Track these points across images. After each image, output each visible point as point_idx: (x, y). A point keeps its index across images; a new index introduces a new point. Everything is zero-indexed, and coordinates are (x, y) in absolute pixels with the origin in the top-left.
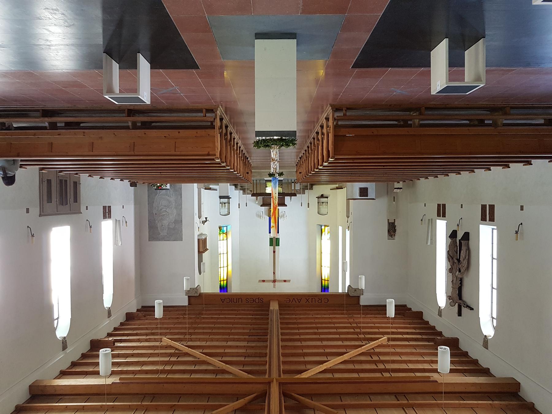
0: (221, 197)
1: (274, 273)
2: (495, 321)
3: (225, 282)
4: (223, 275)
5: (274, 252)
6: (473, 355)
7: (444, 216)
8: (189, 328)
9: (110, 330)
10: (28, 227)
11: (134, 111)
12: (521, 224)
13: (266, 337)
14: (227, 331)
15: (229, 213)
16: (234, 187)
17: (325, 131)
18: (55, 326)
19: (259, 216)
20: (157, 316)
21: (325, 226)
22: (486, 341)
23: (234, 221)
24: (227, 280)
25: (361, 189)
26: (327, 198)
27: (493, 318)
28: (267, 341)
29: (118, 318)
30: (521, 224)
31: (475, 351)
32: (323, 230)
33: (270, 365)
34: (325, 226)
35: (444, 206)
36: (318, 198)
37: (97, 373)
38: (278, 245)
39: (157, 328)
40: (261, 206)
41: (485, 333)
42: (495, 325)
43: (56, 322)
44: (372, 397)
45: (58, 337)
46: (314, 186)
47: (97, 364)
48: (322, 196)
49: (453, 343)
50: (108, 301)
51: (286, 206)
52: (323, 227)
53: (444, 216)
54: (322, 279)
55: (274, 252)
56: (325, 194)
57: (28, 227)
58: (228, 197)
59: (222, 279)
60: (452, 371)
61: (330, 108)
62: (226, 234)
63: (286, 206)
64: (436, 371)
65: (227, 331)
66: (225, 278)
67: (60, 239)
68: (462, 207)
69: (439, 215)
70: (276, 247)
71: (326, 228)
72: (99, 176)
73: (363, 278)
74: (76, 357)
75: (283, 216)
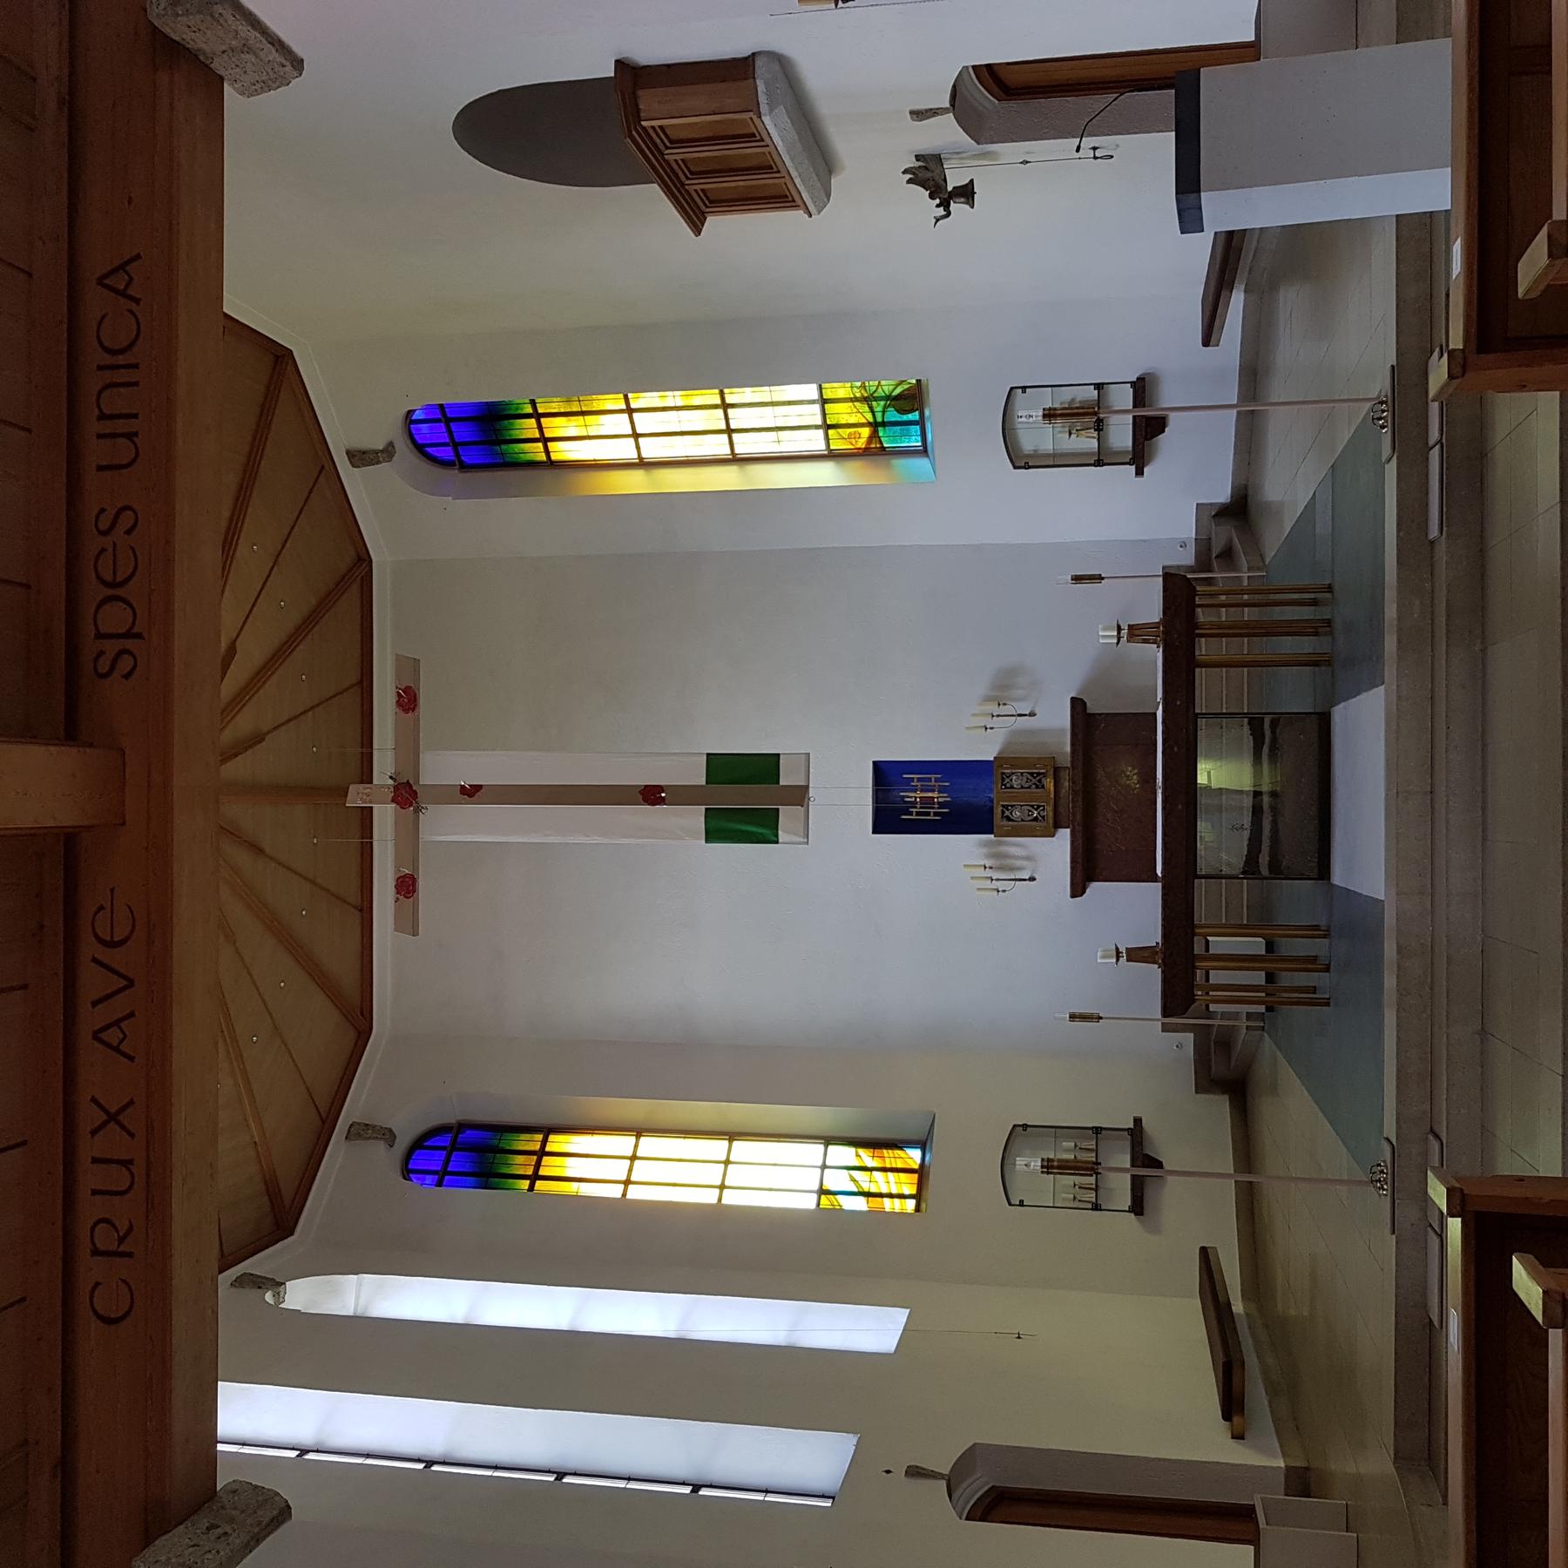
0: (1142, 388)
1: (471, 792)
3: (536, 452)
4: (590, 435)
5: (652, 795)
11: (1192, 607)
15: (1021, 460)
16: (1223, 495)
19: (1002, 690)
21: (922, 1173)
23: (969, 499)
24: (551, 464)
26: (1137, 1207)
32: (893, 1158)
34: (922, 1173)
36: (1136, 1133)
38: (721, 828)
40: (1077, 704)
46: (1220, 1106)
48: (1145, 1160)
51: (1078, 890)
52: (914, 1156)
54: (548, 1131)
55: (652, 795)
56: (1172, 1196)
58: (1139, 459)
59: (555, 427)
62: (873, 452)
63: (1078, 890)
66: (561, 452)
70: (696, 817)
71: (908, 1185)
75: (1003, 864)
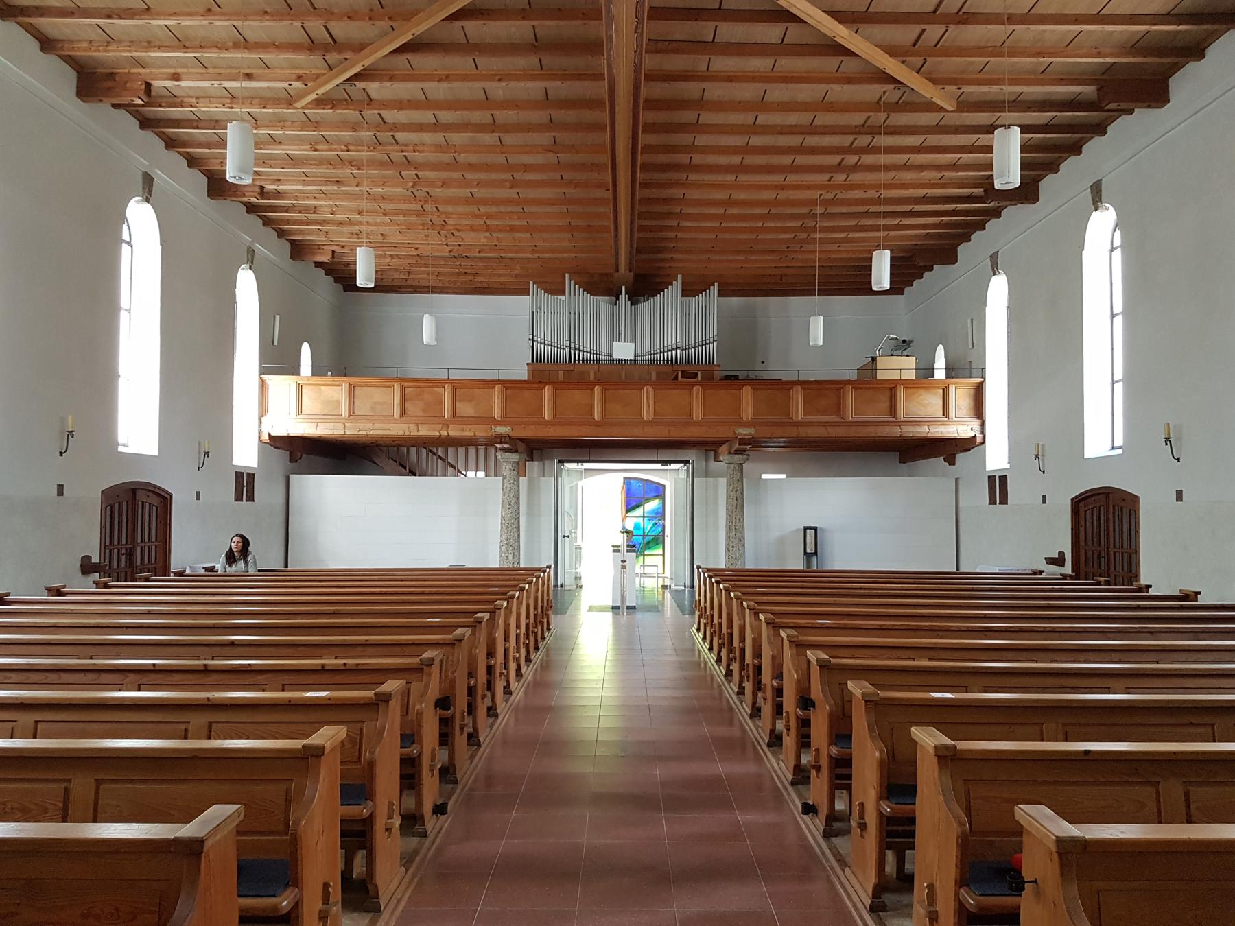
2: (125, 236)
6: (175, 160)
7: (239, 475)
8: (814, 229)
9: (992, 225)
10: (1178, 459)
12: (61, 454)
13: (641, 235)
14: (735, 211)
17: (513, 666)
18: (1118, 233)
20: (887, 254)
22: (148, 188)
25: (625, 478)
27: (129, 243)
28: (646, 101)
29: (971, 252)
30: (61, 454)
31: (173, 175)
33: (633, 181)
35: (238, 498)
37: (1025, 129)
39: (887, 228)
41: (148, 208)
42: (125, 227)
43: (1117, 242)
44: (421, 97)
45: (1112, 210)
47: (1024, 148)
49: (218, 186)
50: (998, 288)
53: (239, 475)
57: (1178, 459)
60: (217, 123)
61: (481, 739)
64: (256, 121)
65: (735, 211)
67: (1102, 431)
68: (198, 493)
69: (251, 477)
72: (1044, 575)
73: (426, 340)
74: (1070, 165)
